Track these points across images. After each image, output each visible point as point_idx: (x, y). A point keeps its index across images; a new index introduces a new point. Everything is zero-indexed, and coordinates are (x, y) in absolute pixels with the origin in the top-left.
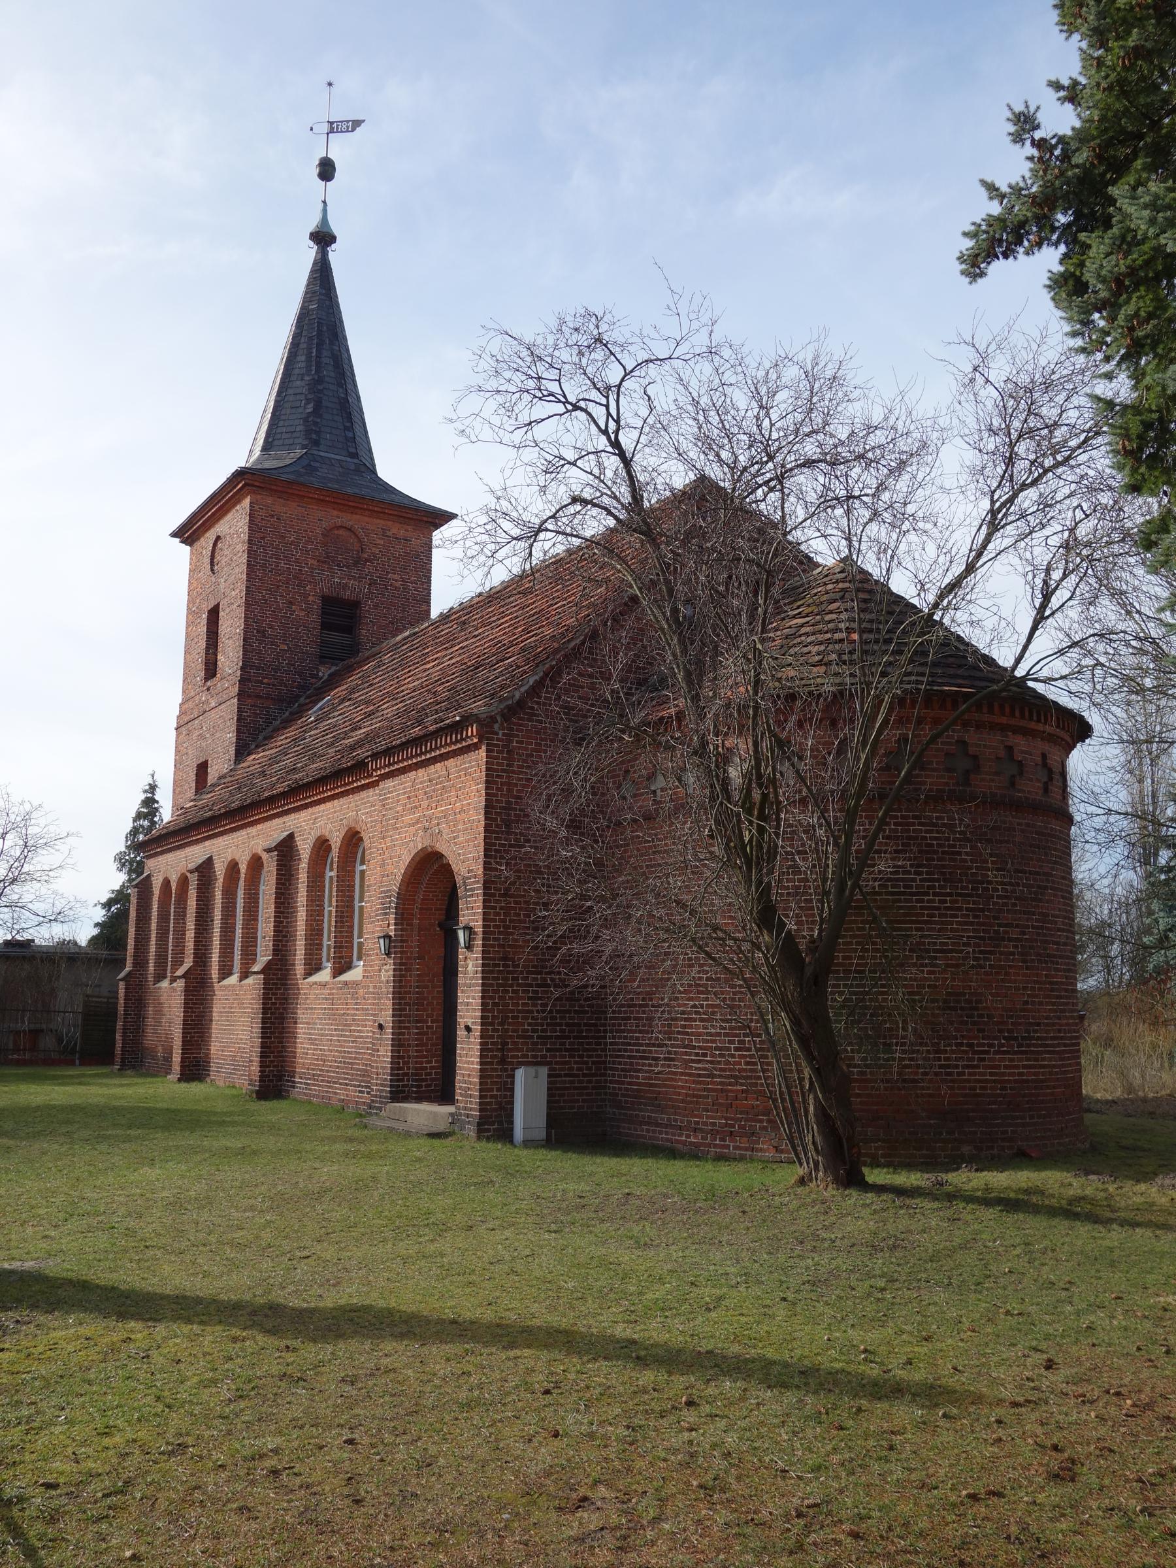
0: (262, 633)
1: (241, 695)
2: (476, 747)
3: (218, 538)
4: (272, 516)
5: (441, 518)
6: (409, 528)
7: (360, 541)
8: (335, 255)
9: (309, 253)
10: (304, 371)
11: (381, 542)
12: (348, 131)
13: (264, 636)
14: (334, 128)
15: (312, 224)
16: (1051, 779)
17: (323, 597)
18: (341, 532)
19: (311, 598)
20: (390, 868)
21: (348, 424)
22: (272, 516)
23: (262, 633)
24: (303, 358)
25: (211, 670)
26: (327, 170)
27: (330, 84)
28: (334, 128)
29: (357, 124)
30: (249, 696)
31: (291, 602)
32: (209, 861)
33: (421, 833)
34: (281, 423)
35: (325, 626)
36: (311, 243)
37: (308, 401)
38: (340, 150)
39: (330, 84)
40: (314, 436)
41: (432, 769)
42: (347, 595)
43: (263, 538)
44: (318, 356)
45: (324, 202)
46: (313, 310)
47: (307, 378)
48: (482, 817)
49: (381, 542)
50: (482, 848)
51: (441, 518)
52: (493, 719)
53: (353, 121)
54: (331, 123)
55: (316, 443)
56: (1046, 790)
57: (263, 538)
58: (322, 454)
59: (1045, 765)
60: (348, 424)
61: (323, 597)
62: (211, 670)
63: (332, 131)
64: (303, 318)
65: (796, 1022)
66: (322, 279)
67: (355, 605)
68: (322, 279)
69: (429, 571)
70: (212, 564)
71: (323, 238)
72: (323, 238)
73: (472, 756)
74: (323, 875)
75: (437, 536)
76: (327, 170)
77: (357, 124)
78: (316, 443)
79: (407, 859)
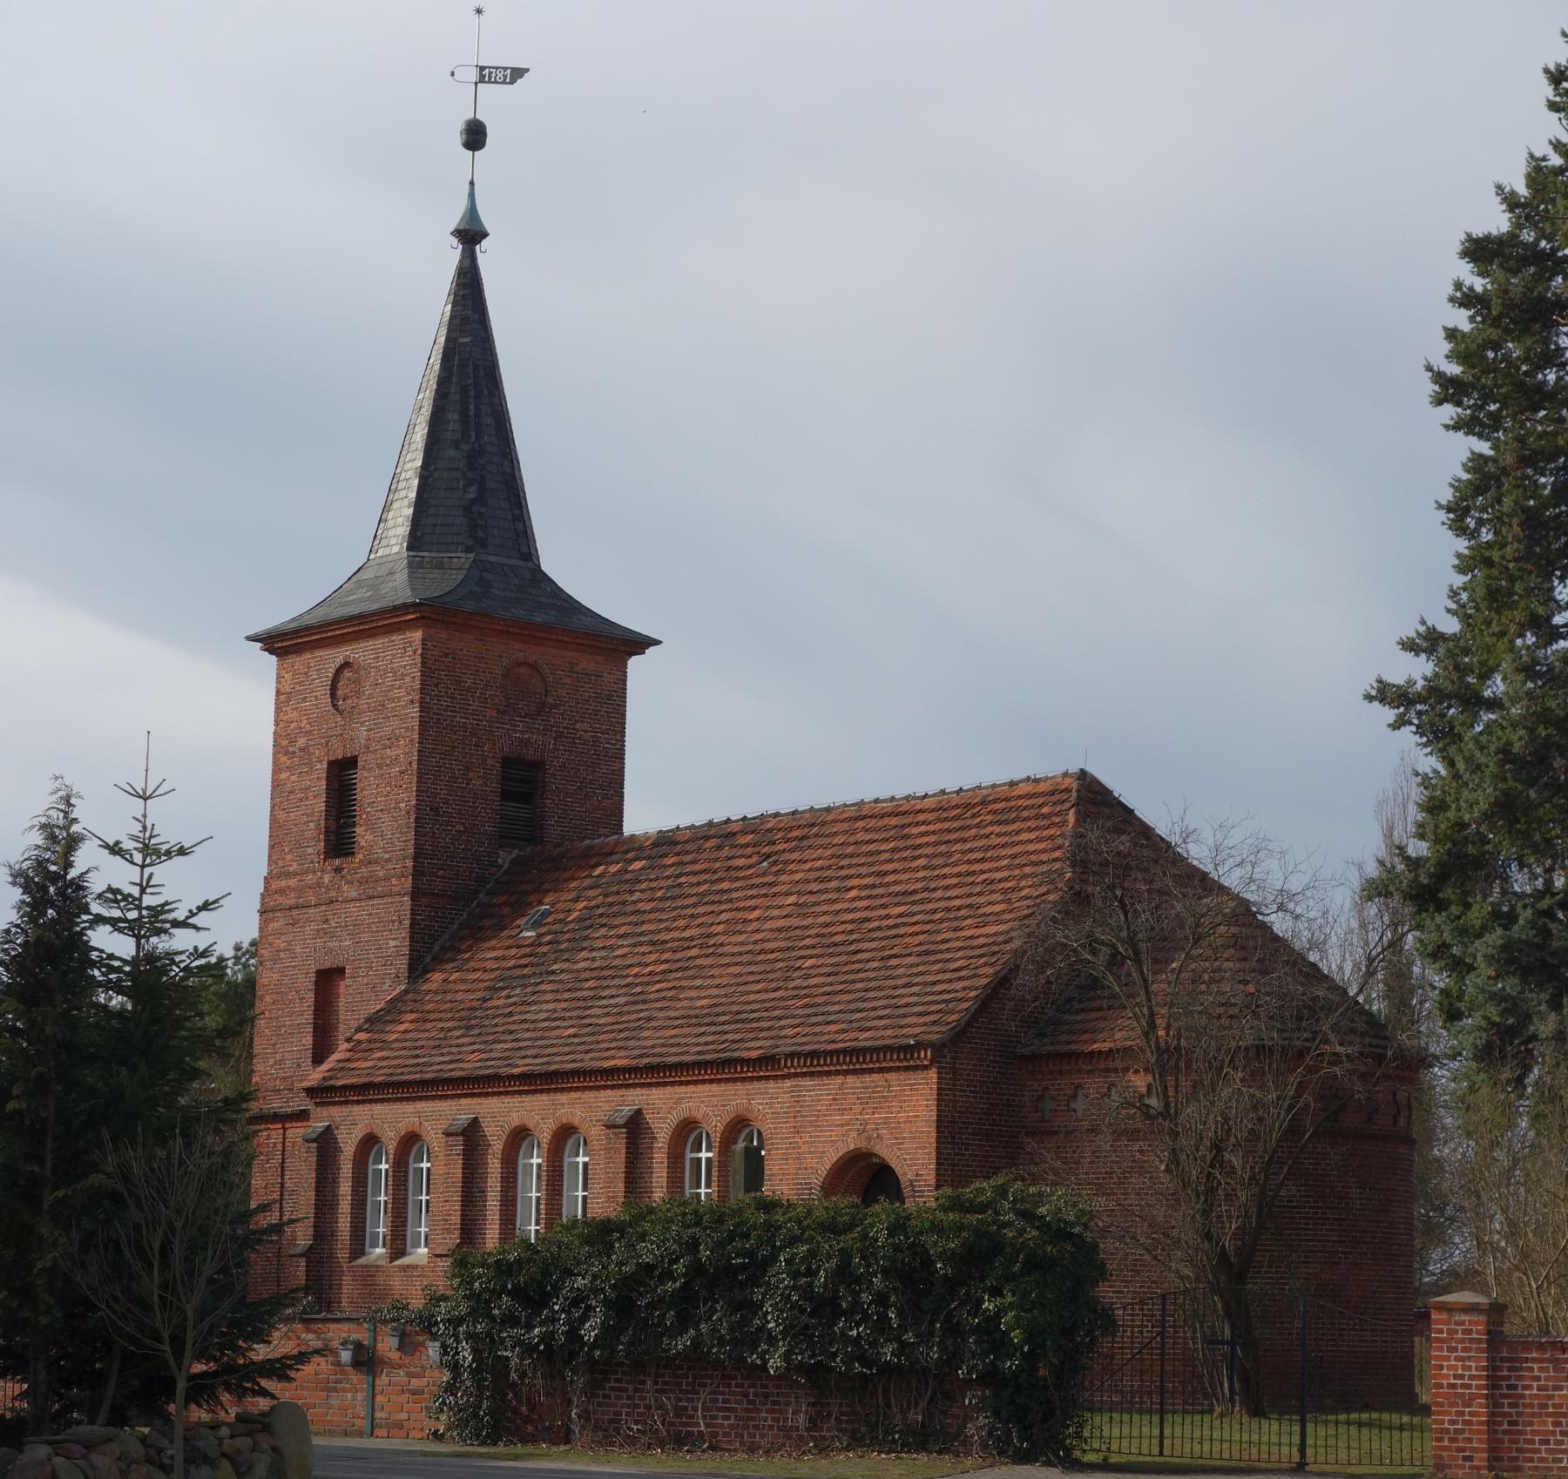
0: (435, 809)
1: (415, 894)
2: (926, 1068)
3: (347, 664)
4: (446, 655)
5: (640, 644)
6: (601, 659)
7: (544, 680)
8: (488, 258)
9: (453, 254)
10: (458, 436)
11: (568, 681)
12: (504, 82)
13: (438, 814)
14: (485, 75)
15: (454, 216)
16: (1399, 1111)
17: (503, 758)
18: (522, 670)
19: (489, 761)
20: (810, 1161)
21: (517, 512)
22: (446, 655)
23: (435, 809)
24: (456, 416)
25: (339, 841)
26: (475, 136)
27: (479, 11)
28: (485, 75)
29: (517, 73)
30: (424, 894)
31: (467, 768)
32: (475, 1124)
33: (854, 1134)
34: (432, 511)
35: (506, 796)
36: (455, 241)
37: (469, 482)
38: (494, 106)
39: (479, 11)
40: (480, 533)
41: (867, 1078)
42: (530, 754)
43: (436, 685)
44: (477, 416)
45: (472, 183)
46: (465, 344)
47: (465, 447)
48: (933, 1129)
49: (568, 681)
50: (934, 1155)
51: (640, 644)
52: (944, 1045)
53: (513, 69)
54: (482, 69)
55: (483, 543)
56: (1395, 1122)
57: (436, 685)
58: (492, 559)
59: (1395, 1100)
60: (517, 512)
61: (503, 758)
62: (339, 841)
63: (482, 80)
64: (450, 353)
65: (1226, 1304)
66: (468, 292)
67: (538, 765)
68: (468, 292)
69: (624, 715)
70: (333, 696)
71: (470, 235)
72: (470, 235)
73: (920, 1075)
74: (683, 1156)
75: (635, 664)
76: (475, 136)
77: (517, 73)
78: (483, 543)
79: (833, 1156)
